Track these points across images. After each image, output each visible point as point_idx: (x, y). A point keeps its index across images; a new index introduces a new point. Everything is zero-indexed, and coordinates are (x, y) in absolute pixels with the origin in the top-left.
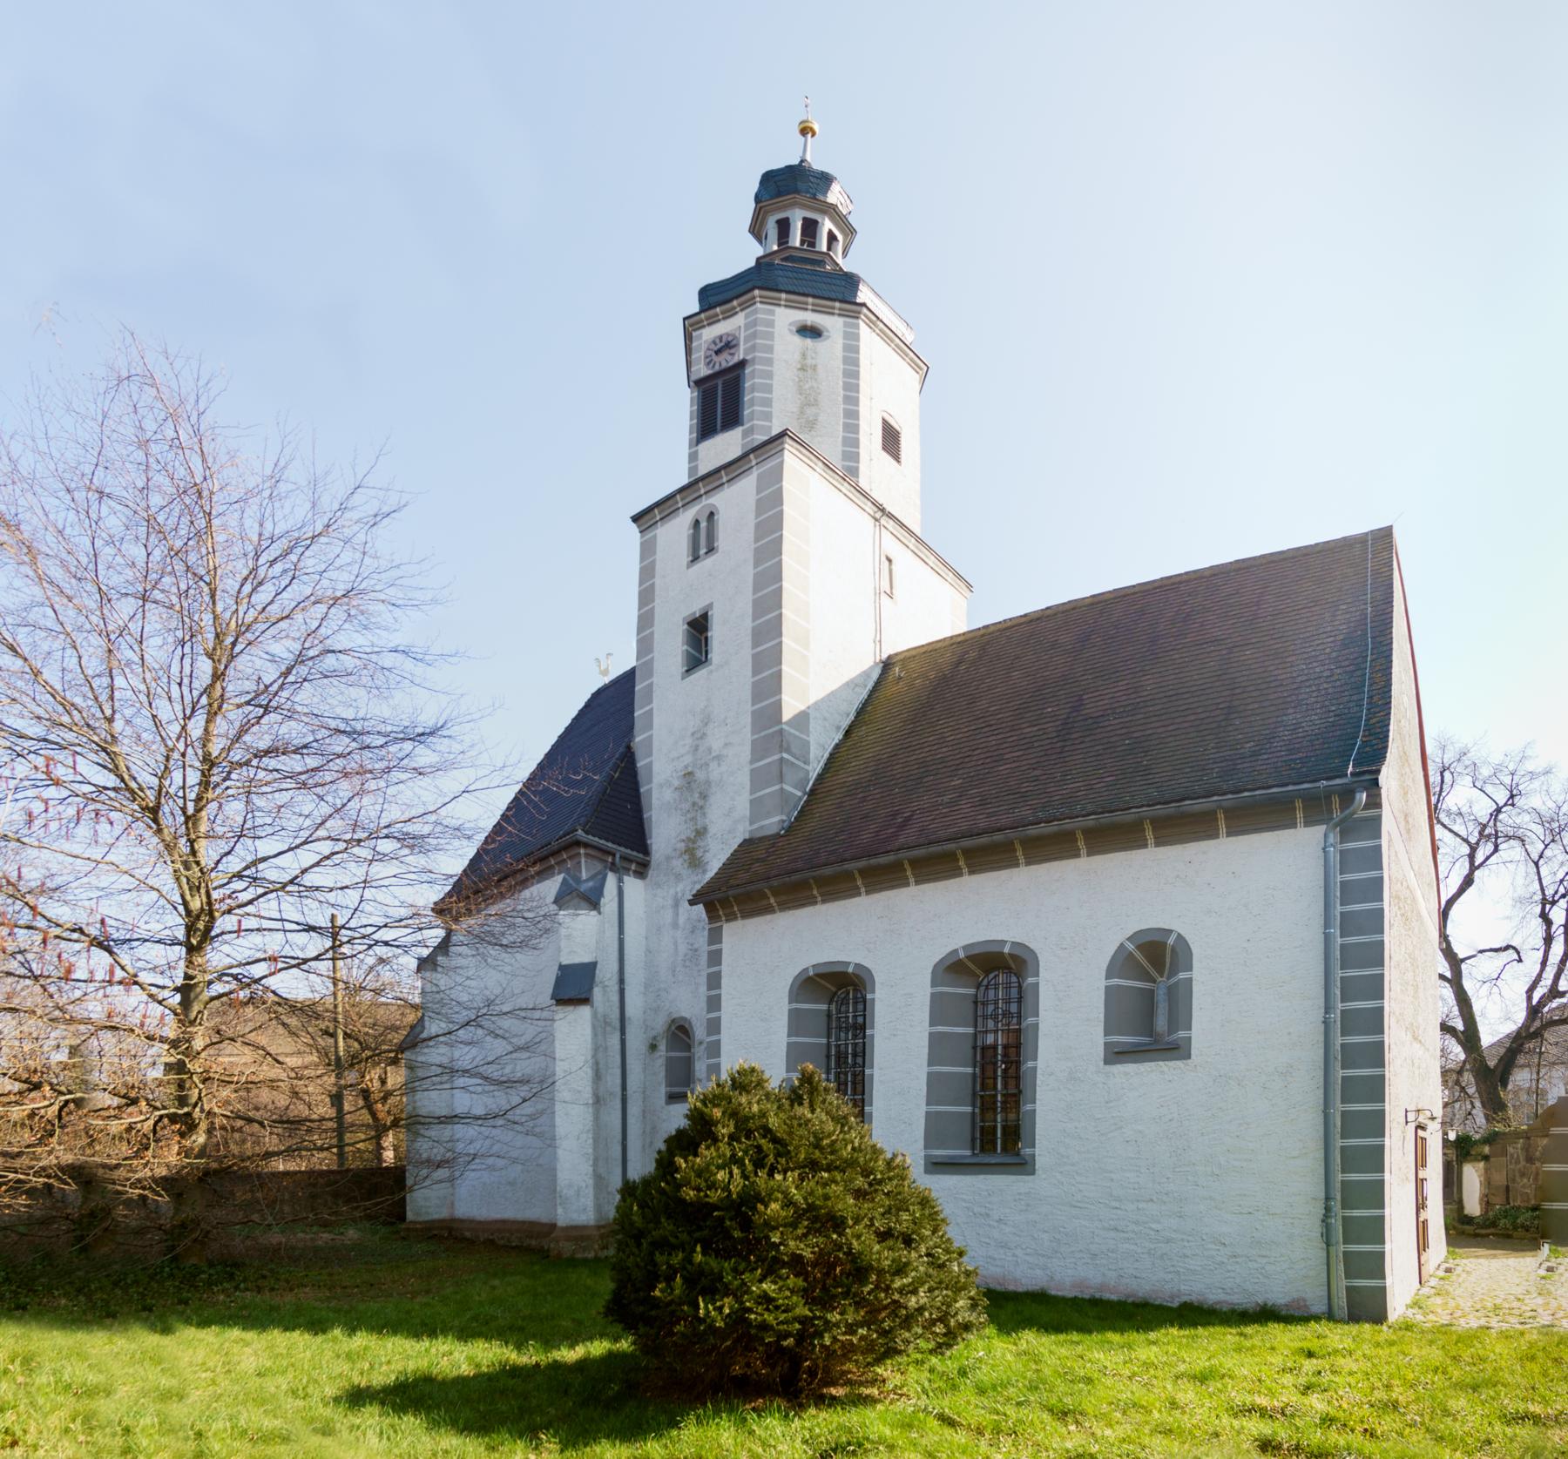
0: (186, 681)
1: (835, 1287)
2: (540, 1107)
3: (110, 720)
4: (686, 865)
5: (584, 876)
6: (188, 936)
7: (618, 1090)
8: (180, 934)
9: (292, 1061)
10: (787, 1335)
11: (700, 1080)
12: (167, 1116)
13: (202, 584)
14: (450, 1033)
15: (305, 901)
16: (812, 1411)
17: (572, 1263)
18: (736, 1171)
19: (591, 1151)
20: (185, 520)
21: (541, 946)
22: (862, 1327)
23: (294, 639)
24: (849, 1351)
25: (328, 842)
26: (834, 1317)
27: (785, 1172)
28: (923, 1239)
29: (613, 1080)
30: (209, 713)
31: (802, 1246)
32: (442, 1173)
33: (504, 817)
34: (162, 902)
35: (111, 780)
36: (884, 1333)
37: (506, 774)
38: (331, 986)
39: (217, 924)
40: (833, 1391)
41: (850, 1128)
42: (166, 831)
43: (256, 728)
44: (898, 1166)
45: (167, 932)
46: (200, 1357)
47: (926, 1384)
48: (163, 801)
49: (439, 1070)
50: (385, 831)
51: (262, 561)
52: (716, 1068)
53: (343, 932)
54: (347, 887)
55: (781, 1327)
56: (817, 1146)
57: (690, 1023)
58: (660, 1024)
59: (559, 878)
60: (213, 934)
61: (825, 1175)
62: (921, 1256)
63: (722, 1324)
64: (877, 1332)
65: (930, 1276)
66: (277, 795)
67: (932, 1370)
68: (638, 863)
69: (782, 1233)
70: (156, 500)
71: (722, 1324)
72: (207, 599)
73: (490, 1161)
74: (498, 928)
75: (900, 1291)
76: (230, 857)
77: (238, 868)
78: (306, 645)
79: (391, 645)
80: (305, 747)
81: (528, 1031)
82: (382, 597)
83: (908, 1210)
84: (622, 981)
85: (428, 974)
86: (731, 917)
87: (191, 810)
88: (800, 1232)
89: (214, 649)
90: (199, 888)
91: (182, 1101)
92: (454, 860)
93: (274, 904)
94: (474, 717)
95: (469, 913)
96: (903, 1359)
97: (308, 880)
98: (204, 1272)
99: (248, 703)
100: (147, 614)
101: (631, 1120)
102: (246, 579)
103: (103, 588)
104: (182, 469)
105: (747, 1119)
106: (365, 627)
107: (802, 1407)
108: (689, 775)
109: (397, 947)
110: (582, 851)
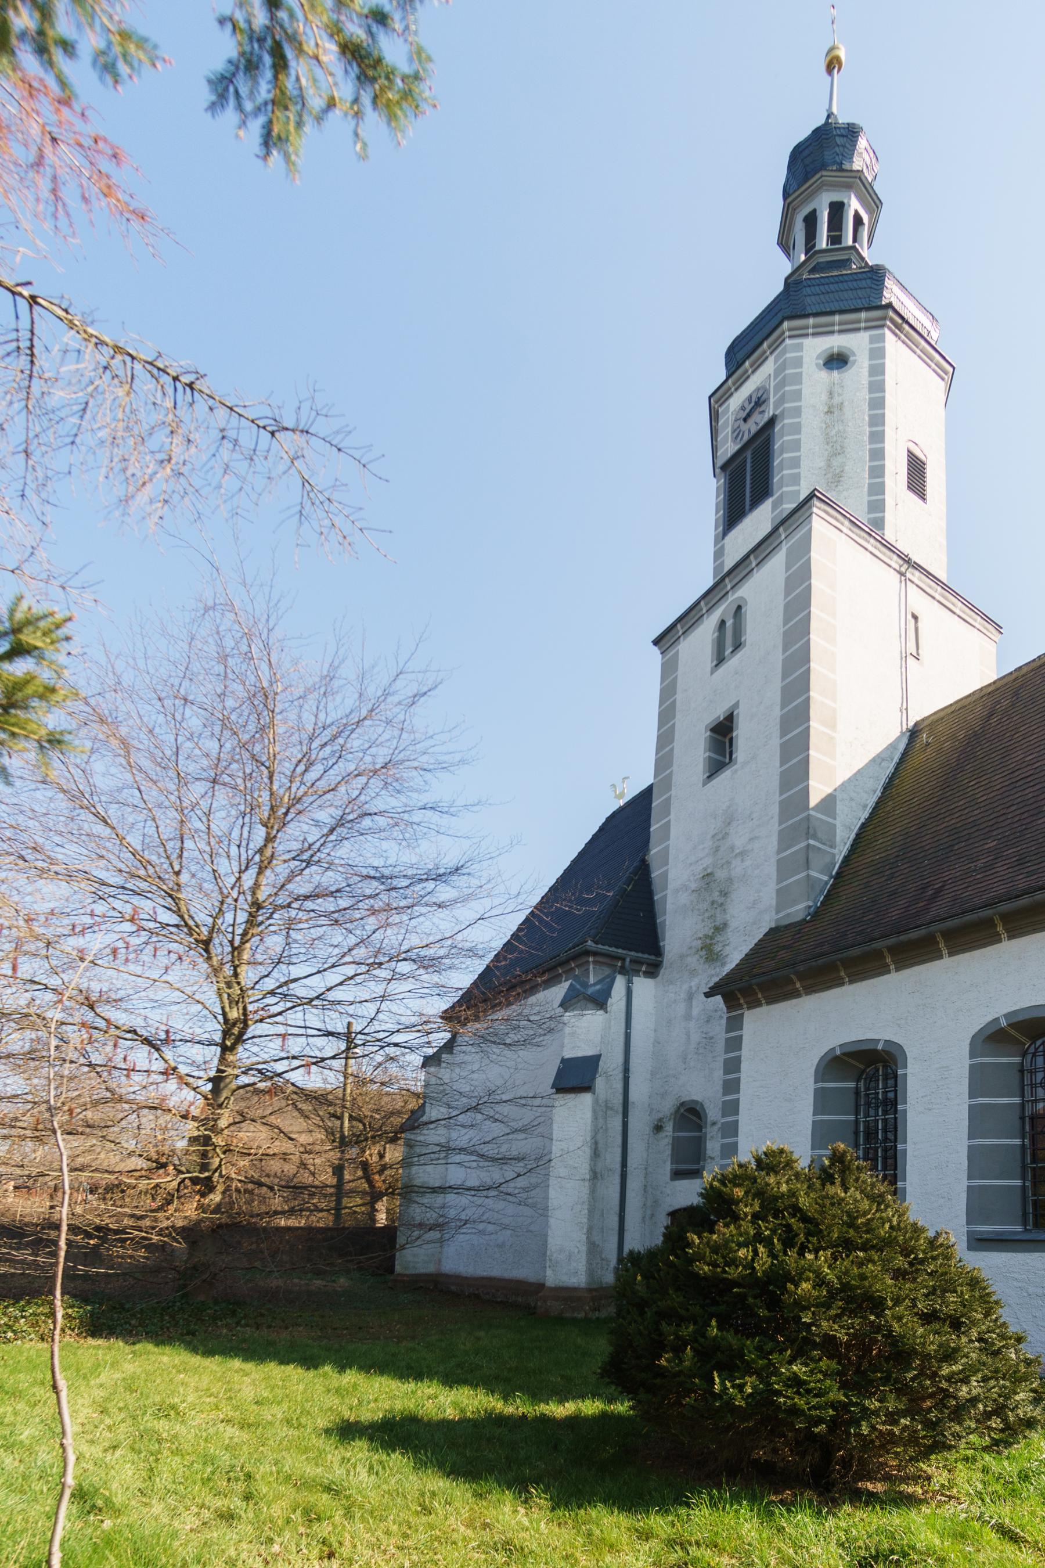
0: (244, 843)
1: (874, 1372)
2: (533, 1181)
3: (178, 873)
4: (702, 961)
5: (592, 980)
6: (224, 1039)
7: (618, 1167)
8: (218, 1037)
9: (303, 1139)
10: (819, 1421)
11: (712, 1158)
12: (190, 1179)
13: (263, 768)
14: (450, 1118)
15: (327, 1012)
16: (847, 1508)
17: (560, 1321)
18: (761, 1249)
19: (586, 1220)
20: (253, 718)
21: (544, 1043)
22: (905, 1417)
23: (336, 807)
24: (889, 1442)
25: (353, 966)
26: (873, 1404)
27: (816, 1252)
28: (974, 1323)
29: (613, 1157)
30: (260, 868)
31: (836, 1327)
32: (434, 1235)
33: (515, 936)
34: (205, 1012)
35: (174, 919)
36: (930, 1425)
37: (520, 901)
38: (342, 1079)
39: (250, 1030)
40: (870, 1486)
41: (887, 1206)
42: (215, 959)
43: (298, 878)
44: (941, 1245)
45: (207, 1036)
46: (204, 1384)
47: (980, 1486)
48: (215, 935)
49: (438, 1148)
50: (403, 956)
51: (314, 745)
52: (731, 1149)
53: (359, 1036)
54: (366, 1001)
55: (813, 1413)
56: (851, 1224)
57: (702, 1105)
58: (667, 1107)
59: (565, 985)
60: (245, 1037)
61: (861, 1254)
62: (971, 1341)
63: (743, 1403)
64: (921, 1423)
65: (984, 1364)
66: (312, 930)
67: (985, 1470)
68: (648, 964)
69: (813, 1313)
70: (230, 703)
71: (743, 1403)
72: (266, 780)
73: (481, 1226)
74: (502, 1028)
75: (949, 1379)
76: (266, 979)
77: (272, 987)
78: (347, 811)
79: (420, 804)
80: (338, 891)
81: (527, 1116)
82: (416, 764)
83: (956, 1292)
84: (626, 1070)
85: (432, 1069)
86: (754, 1004)
87: (237, 943)
88: (833, 1312)
89: (269, 819)
90: (237, 1003)
91: (204, 1167)
92: (463, 977)
93: (300, 1015)
94: (493, 855)
95: (477, 1019)
96: (952, 1456)
97: (331, 996)
98: (209, 1308)
99: (294, 859)
100: (216, 793)
101: (630, 1195)
102: (300, 761)
103: (182, 774)
104: (253, 677)
105: (776, 1198)
106: (399, 792)
107: (835, 1503)
108: (708, 877)
109: (405, 1047)
110: (591, 959)
